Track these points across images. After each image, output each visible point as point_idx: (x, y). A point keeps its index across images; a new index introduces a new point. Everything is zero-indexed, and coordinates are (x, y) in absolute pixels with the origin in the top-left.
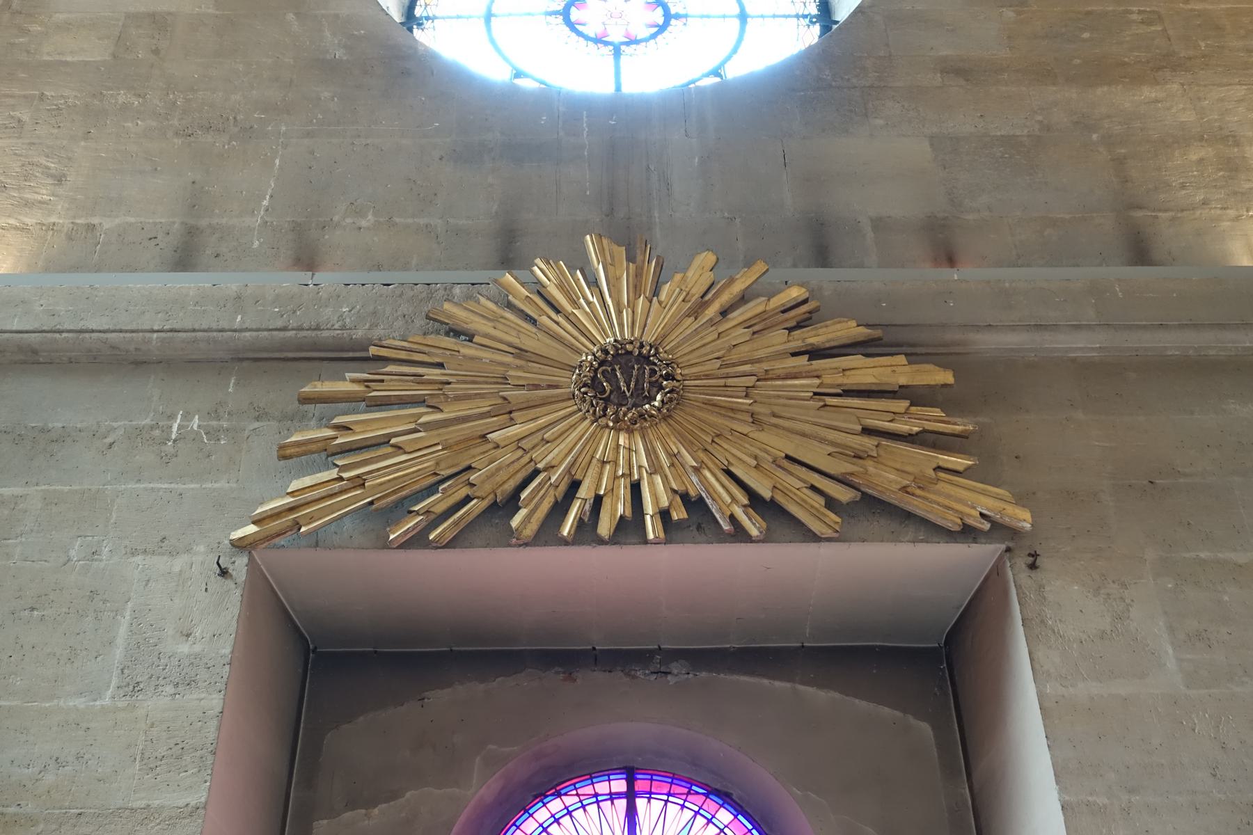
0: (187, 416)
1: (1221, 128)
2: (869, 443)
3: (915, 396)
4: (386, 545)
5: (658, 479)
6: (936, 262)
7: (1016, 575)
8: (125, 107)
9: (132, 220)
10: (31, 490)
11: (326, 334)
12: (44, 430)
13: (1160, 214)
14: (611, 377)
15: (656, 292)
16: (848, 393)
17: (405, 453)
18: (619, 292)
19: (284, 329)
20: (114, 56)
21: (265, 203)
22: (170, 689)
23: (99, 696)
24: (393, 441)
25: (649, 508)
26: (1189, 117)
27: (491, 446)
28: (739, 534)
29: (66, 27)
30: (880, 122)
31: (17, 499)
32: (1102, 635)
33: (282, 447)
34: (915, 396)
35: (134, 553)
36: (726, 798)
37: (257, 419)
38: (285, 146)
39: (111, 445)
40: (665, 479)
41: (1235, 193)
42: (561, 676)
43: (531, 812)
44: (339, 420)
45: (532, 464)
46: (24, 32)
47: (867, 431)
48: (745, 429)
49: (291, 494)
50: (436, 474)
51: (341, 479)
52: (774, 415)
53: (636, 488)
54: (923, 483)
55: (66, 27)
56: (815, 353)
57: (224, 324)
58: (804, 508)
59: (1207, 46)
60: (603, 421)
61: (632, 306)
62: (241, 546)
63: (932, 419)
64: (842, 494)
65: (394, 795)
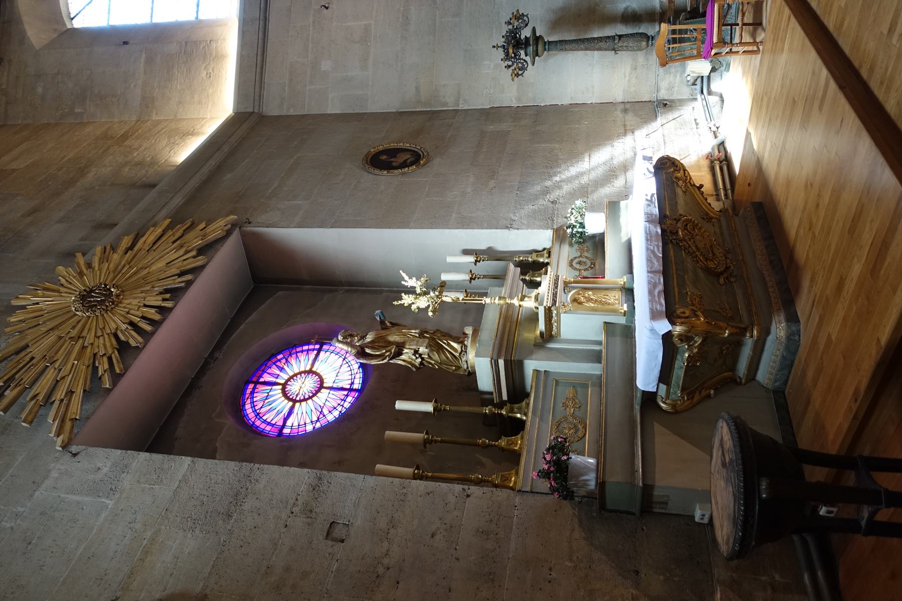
4: (109, 391)
17: (68, 376)
27: (90, 346)
28: (189, 283)
42: (197, 390)
43: (246, 415)
45: (110, 335)
50: (88, 366)
60: (109, 308)
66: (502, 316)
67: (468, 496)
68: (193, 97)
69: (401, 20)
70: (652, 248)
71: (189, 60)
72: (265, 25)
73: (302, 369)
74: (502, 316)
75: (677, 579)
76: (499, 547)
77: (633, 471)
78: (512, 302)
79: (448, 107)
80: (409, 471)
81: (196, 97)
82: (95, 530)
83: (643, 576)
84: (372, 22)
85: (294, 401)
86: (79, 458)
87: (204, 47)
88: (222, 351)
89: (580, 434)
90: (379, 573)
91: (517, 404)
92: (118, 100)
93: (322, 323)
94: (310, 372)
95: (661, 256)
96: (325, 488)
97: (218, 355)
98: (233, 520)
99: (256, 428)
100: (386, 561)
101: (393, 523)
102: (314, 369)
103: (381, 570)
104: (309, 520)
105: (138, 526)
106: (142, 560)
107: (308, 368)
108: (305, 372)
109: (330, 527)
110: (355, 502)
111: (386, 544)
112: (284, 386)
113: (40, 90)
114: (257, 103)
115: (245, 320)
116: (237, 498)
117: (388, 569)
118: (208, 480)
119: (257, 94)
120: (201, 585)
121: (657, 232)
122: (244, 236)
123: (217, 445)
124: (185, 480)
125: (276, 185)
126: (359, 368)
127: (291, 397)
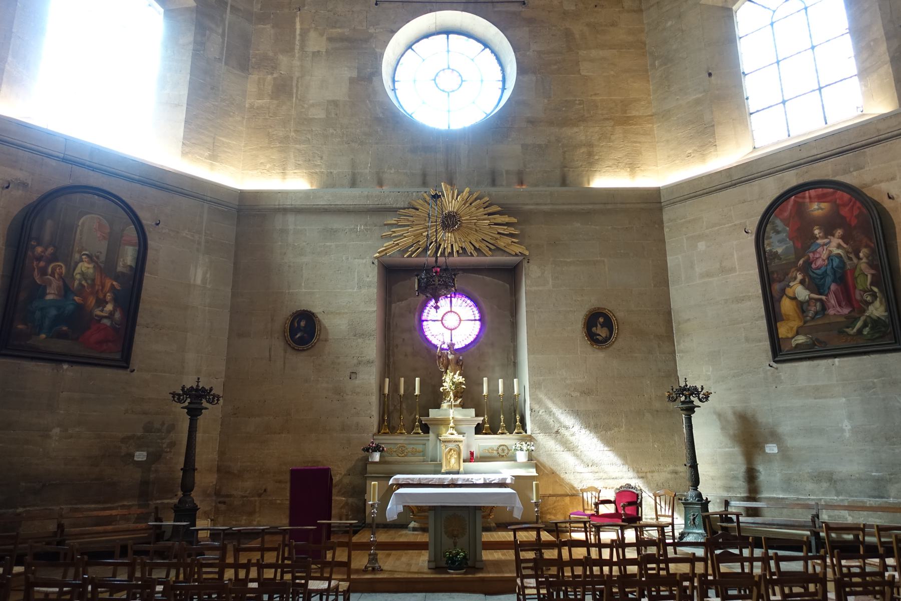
0: (361, 226)
1: (590, 142)
2: (498, 236)
3: (508, 224)
5: (456, 244)
6: (519, 185)
7: (525, 264)
8: (332, 134)
9: (340, 170)
10: (332, 244)
11: (387, 206)
12: (332, 229)
13: (571, 169)
14: (447, 221)
15: (457, 199)
16: (495, 224)
18: (449, 198)
19: (378, 204)
20: (326, 116)
21: (369, 165)
22: (367, 288)
23: (354, 289)
24: (404, 235)
25: (455, 250)
26: (583, 138)
29: (313, 105)
30: (510, 139)
31: (330, 246)
32: (539, 277)
33: (382, 236)
34: (508, 224)
35: (355, 259)
36: (469, 298)
37: (375, 226)
38: (371, 147)
39: (346, 233)
40: (458, 244)
41: (589, 163)
44: (392, 230)
46: (303, 107)
47: (499, 233)
48: (474, 232)
49: (385, 247)
51: (394, 244)
52: (480, 229)
53: (452, 245)
54: (509, 245)
55: (313, 105)
56: (489, 214)
57: (365, 203)
58: (485, 250)
59: (593, 113)
61: (452, 202)
62: (376, 258)
63: (512, 230)
64: (493, 247)
65: (406, 299)
68: (672, 150)
69: (741, 295)
71: (699, 134)
72: (730, 186)
77: (371, 473)
79: (677, 346)
80: (386, 391)
81: (672, 152)
84: (737, 273)
85: (442, 320)
87: (710, 142)
89: (400, 455)
92: (667, 91)
93: (488, 318)
100: (345, 395)
101: (358, 394)
103: (342, 394)
106: (337, 314)
111: (350, 393)
112: (451, 311)
113: (669, 23)
114: (668, 203)
116: (362, 335)
119: (675, 200)
122: (521, 262)
124: (367, 312)
125: (568, 260)
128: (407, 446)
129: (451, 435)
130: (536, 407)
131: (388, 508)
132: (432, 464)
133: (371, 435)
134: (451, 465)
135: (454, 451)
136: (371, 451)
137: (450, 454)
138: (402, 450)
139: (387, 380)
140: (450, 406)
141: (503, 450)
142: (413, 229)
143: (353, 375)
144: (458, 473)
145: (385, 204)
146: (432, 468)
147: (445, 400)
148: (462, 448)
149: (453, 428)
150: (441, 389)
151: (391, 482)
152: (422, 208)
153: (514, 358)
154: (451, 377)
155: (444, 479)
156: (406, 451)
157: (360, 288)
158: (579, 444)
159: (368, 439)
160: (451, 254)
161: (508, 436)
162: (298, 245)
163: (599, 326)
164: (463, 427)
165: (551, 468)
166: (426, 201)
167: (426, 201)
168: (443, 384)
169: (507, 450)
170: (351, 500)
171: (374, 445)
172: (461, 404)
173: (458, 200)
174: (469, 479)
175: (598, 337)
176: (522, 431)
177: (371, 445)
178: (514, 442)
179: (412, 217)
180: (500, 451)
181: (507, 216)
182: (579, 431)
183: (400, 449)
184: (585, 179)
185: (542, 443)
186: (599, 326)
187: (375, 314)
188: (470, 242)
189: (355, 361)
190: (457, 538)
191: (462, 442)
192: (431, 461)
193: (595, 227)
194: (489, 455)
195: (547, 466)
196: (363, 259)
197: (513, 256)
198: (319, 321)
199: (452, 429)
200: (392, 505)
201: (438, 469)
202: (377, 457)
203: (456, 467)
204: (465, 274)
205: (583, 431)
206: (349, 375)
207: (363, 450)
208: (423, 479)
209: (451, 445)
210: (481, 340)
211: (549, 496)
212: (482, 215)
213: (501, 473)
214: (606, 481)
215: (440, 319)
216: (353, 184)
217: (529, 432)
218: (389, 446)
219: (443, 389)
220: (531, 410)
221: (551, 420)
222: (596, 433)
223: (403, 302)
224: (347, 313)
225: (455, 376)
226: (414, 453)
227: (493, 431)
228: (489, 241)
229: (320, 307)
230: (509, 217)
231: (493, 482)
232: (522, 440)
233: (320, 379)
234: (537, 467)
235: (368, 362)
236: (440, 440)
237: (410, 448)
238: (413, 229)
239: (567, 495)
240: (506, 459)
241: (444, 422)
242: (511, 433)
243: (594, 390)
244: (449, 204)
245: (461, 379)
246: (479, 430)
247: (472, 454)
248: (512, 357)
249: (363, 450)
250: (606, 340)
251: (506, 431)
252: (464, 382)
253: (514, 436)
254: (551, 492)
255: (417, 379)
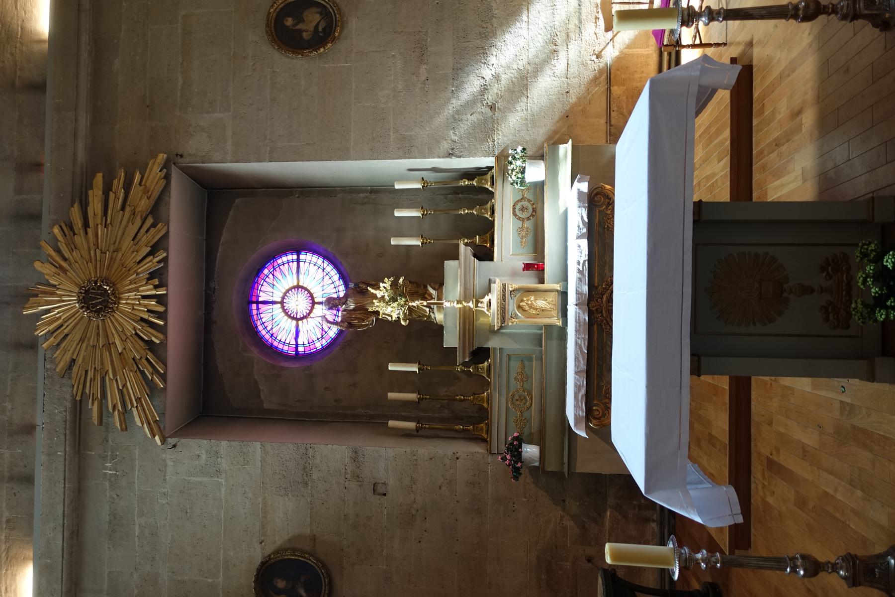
0: (106, 468)
2: (128, 209)
3: (108, 188)
4: (165, 389)
5: (141, 289)
7: (185, 162)
11: (68, 418)
14: (95, 305)
15: (54, 286)
18: (53, 301)
19: (65, 435)
22: (219, 460)
24: (121, 388)
25: (154, 292)
27: (124, 351)
32: (209, 137)
33: (122, 430)
34: (108, 188)
36: (260, 271)
37: (107, 441)
42: (214, 326)
44: (111, 409)
47: (123, 208)
49: (143, 424)
51: (137, 407)
52: (115, 243)
56: (86, 225)
58: (155, 235)
60: (115, 309)
61: (61, 296)
62: (164, 441)
63: (118, 184)
66: (461, 314)
67: (458, 458)
70: (580, 342)
73: (291, 285)
74: (461, 314)
75: (586, 504)
76: (482, 492)
77: (563, 463)
78: (468, 304)
80: (411, 425)
82: (224, 501)
83: (567, 503)
85: (297, 320)
86: (178, 448)
88: (216, 280)
90: (413, 514)
91: (481, 364)
93: (293, 237)
94: (298, 287)
95: (586, 352)
96: (362, 459)
97: (214, 286)
98: (310, 487)
99: (276, 349)
101: (413, 481)
102: (301, 284)
103: (414, 512)
104: (359, 483)
105: (250, 495)
106: (265, 517)
107: (295, 284)
108: (294, 287)
109: (374, 486)
110: (385, 468)
111: (412, 495)
112: (282, 303)
115: (220, 241)
116: (306, 470)
117: (418, 511)
118: (280, 459)
120: (309, 529)
121: (585, 319)
123: (256, 377)
124: (263, 460)
125: (181, 81)
126: (339, 280)
127: (292, 315)
128: (512, 390)
129: (149, 233)
130: (445, 146)
131: (698, 520)
132: (546, 342)
133: (490, 459)
134: (548, 307)
135: (522, 301)
136: (519, 465)
137: (527, 308)
138: (520, 399)
139: (391, 423)
140: (440, 306)
141: (523, 209)
142: (110, 372)
143: (378, 489)
144: (564, 294)
145: (65, 421)
146: (554, 344)
147: (429, 317)
148: (516, 286)
149: (477, 302)
150: (403, 323)
151: (583, 434)
152: (70, 352)
153: (363, 193)
154: (382, 304)
155: (578, 322)
156: (521, 392)
157: (219, 472)
158: (515, 67)
159: (496, 464)
160: (161, 300)
161: (497, 201)
162: (137, 587)
163: (301, 26)
164: (479, 283)
165: (558, 122)
166: (58, 345)
167: (58, 345)
168: (394, 318)
169: (522, 203)
170: (611, 501)
171: (508, 457)
172: (437, 287)
173: (56, 283)
174: (579, 269)
175: (320, 29)
176: (488, 176)
177: (507, 462)
178: (509, 188)
179: (86, 372)
180: (524, 215)
181: (90, 192)
182: (491, 67)
183: (518, 403)
184: (36, 48)
185: (511, 137)
186: (301, 26)
187: (268, 446)
188: (139, 262)
189: (353, 485)
190: (785, 286)
191: (504, 286)
192: (541, 346)
193: (123, 33)
194: (530, 237)
195: (553, 129)
196: (166, 466)
197: (168, 184)
198: (277, 552)
199: (480, 305)
200: (691, 505)
201: (555, 334)
202: (531, 451)
203: (553, 298)
204: (215, 276)
205: (492, 60)
206: (378, 497)
207: (516, 478)
208: (577, 365)
209: (511, 306)
210: (330, 250)
211: (610, 125)
212: (87, 239)
213: (566, 212)
214: (584, 17)
215: (294, 322)
216: (28, 480)
217: (490, 161)
218: (512, 425)
219: (405, 320)
220: (450, 155)
221: (470, 118)
222: (494, 35)
223: (261, 388)
224: (264, 498)
225: (379, 296)
226: (525, 377)
227: (487, 228)
228: (138, 227)
229: (252, 549)
230: (92, 188)
231: (586, 220)
232: (504, 173)
233: (384, 553)
234: (556, 140)
235: (355, 460)
236: (501, 327)
237: (515, 385)
238: (110, 372)
239: (609, 90)
240: (540, 205)
241: (468, 319)
242: (491, 194)
243: (418, 37)
244: (64, 301)
245: (386, 284)
246: (485, 254)
247: (528, 267)
248: (361, 195)
249: (516, 478)
250: (325, 13)
251: (489, 205)
252: (392, 279)
253: (498, 191)
254: (603, 121)
255: (392, 367)
